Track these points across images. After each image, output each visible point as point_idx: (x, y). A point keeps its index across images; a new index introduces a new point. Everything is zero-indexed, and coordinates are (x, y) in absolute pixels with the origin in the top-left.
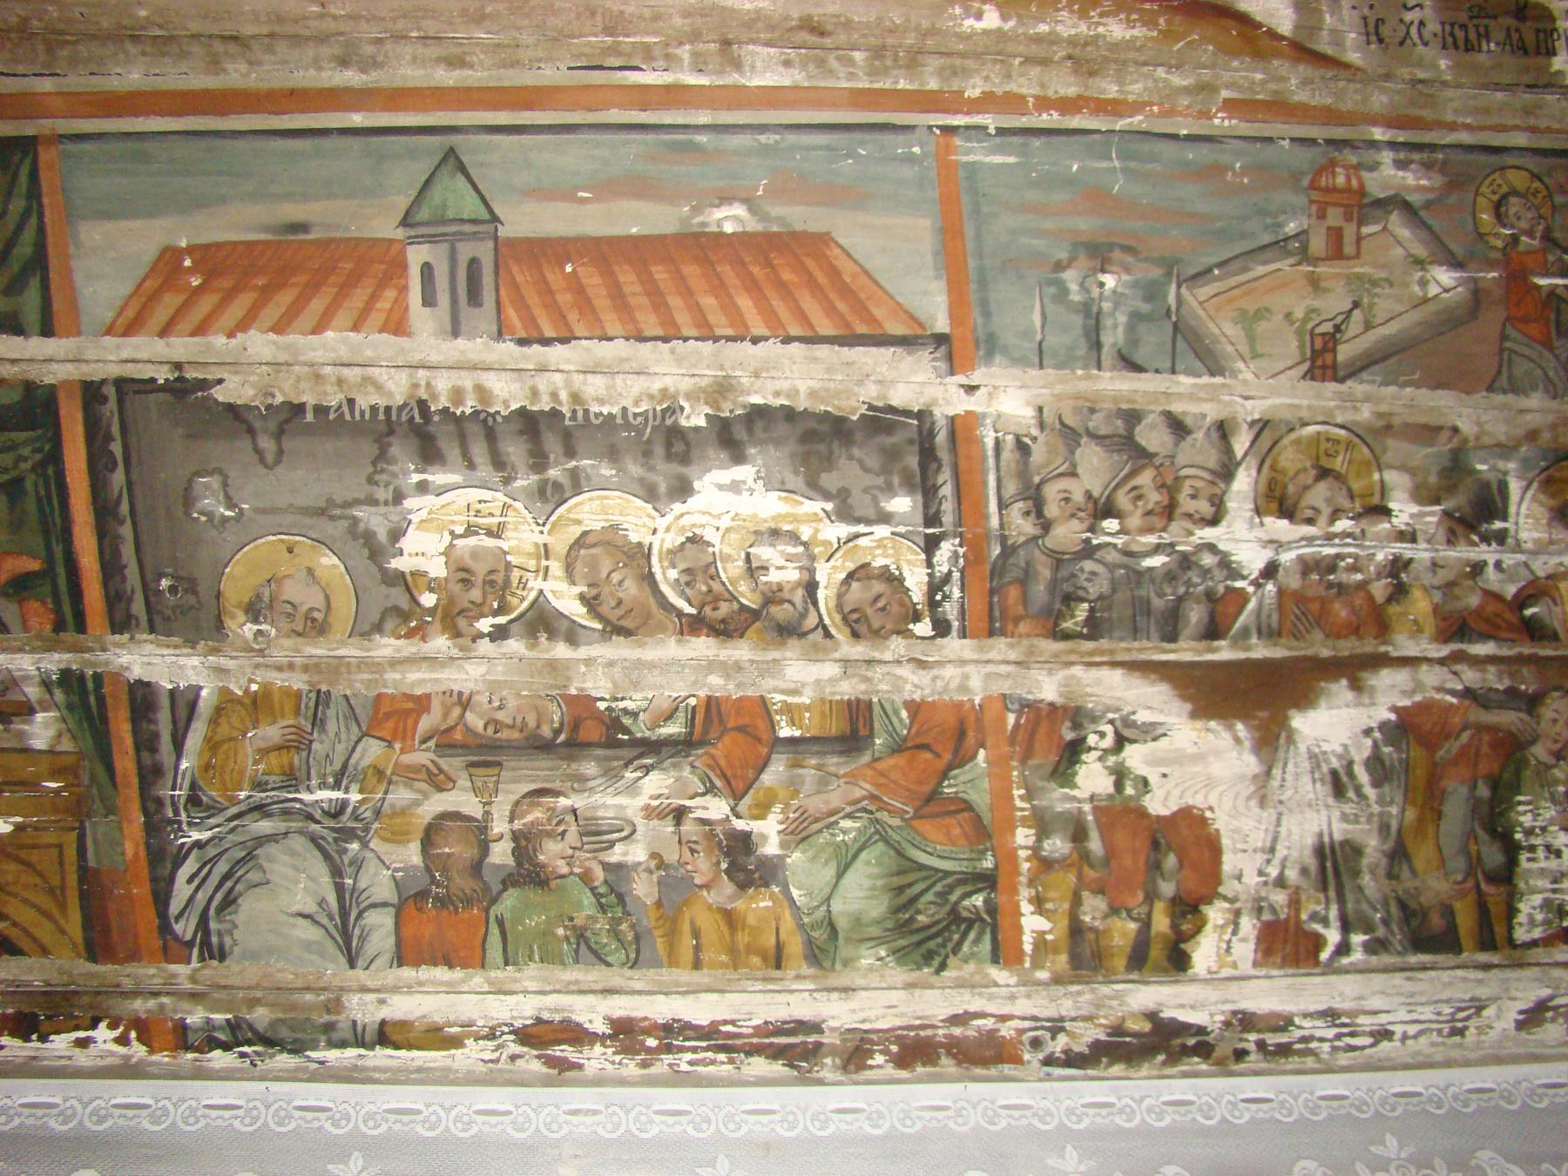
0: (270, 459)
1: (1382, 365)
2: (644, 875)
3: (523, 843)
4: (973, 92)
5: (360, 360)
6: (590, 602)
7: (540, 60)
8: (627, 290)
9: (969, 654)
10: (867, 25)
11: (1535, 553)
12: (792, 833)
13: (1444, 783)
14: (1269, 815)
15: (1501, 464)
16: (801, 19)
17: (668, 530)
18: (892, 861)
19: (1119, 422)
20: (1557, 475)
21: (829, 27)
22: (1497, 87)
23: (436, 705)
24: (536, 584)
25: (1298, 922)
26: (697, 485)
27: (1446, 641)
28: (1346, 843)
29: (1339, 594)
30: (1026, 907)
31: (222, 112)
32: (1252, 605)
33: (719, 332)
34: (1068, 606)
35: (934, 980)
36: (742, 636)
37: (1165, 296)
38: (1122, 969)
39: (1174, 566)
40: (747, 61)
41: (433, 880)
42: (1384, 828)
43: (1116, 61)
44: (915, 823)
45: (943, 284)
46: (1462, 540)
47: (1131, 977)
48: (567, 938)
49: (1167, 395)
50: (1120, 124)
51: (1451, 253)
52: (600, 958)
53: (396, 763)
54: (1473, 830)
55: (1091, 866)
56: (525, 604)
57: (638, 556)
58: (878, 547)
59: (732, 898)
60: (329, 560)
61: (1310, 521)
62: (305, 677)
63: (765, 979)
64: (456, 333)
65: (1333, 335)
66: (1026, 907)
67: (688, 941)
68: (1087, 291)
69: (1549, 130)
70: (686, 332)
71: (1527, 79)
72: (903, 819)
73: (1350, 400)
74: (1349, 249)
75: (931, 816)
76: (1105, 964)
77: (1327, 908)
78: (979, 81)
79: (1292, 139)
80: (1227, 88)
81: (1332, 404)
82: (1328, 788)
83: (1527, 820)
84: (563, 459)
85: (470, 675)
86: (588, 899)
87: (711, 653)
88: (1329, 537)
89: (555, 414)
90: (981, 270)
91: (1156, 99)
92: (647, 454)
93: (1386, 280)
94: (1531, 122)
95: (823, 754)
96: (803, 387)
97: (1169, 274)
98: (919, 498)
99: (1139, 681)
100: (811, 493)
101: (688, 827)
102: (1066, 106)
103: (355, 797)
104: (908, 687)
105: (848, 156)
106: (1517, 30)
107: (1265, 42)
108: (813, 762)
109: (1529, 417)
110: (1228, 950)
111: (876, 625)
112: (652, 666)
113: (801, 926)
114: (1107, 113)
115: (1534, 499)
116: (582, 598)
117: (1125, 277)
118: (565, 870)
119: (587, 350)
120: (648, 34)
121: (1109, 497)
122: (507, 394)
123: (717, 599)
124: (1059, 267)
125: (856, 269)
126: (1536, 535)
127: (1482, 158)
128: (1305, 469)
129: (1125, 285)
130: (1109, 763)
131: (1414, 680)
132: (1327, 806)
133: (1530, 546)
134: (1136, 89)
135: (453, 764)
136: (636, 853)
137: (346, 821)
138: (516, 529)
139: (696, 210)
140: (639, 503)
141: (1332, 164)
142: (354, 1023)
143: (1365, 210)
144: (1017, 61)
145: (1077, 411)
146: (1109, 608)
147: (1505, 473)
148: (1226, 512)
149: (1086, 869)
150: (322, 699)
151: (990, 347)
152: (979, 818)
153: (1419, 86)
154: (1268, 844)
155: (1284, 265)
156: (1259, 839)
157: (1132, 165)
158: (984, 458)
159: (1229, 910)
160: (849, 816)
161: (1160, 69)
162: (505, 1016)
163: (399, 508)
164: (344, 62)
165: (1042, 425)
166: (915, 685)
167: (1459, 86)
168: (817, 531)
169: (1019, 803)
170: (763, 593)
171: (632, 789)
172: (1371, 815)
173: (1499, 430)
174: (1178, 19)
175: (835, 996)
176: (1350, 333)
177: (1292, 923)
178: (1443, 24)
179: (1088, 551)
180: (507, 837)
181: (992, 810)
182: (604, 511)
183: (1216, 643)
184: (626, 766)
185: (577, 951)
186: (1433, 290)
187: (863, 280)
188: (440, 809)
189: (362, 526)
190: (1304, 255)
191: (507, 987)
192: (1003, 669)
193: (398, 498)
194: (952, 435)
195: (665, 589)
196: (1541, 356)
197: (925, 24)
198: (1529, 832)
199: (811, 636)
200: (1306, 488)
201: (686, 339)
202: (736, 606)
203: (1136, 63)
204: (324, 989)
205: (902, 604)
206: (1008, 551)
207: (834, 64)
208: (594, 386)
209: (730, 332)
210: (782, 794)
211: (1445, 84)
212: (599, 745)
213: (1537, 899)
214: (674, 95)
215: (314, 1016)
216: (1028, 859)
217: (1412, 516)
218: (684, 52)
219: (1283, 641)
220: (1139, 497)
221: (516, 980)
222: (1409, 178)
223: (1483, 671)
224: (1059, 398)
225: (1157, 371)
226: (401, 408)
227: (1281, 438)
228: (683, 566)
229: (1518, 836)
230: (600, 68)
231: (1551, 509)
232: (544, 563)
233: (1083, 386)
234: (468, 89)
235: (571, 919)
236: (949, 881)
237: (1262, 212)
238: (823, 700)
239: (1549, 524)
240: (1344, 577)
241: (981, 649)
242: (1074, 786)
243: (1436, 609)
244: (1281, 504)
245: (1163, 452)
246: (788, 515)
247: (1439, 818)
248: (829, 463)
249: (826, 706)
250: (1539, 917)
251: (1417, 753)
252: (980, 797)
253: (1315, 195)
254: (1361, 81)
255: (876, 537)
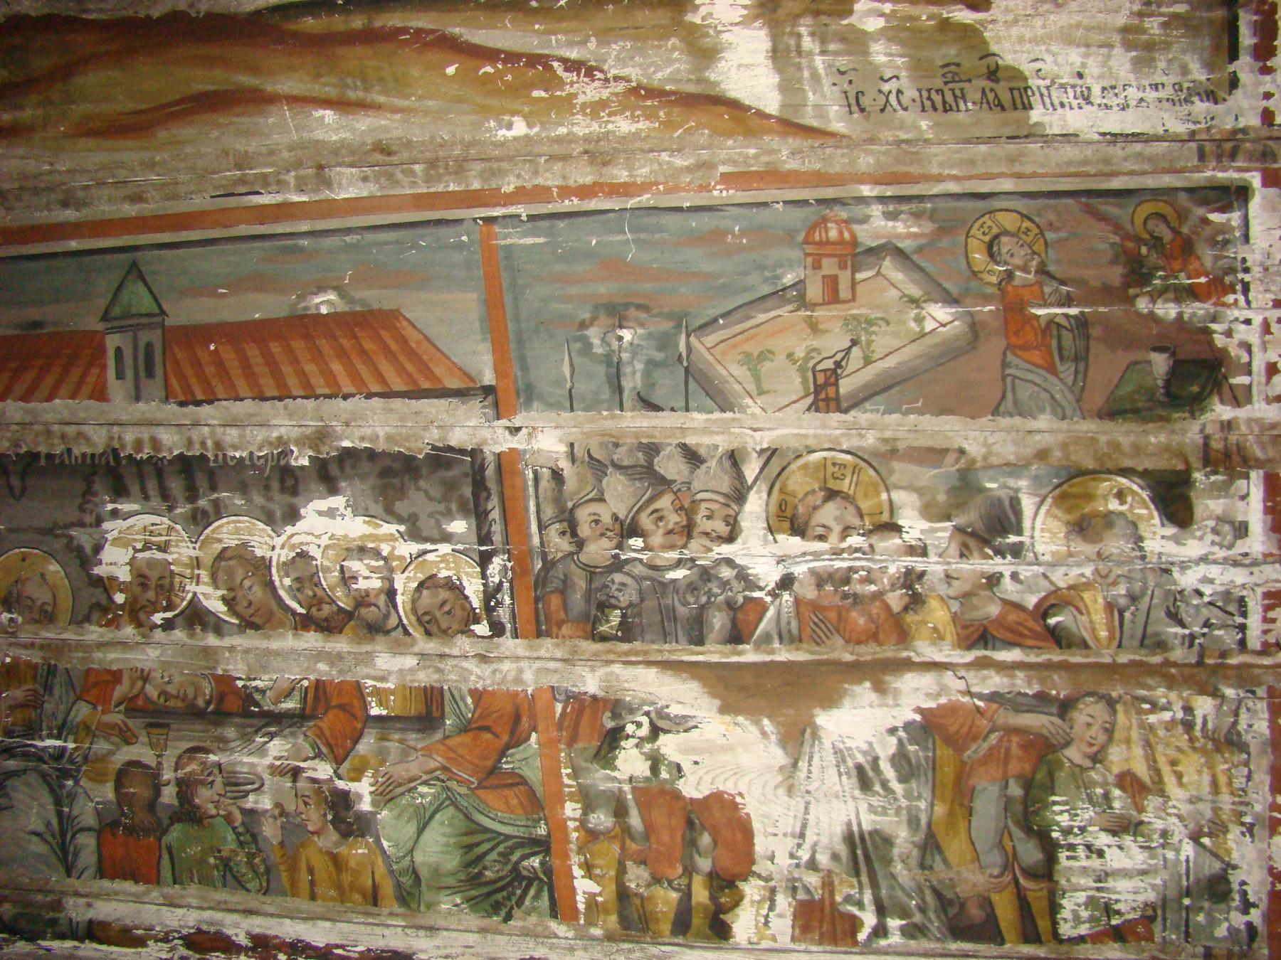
0: (17, 492)
1: (884, 395)
2: (271, 820)
3: (184, 788)
4: (508, 188)
5: (74, 420)
6: (229, 602)
7: (192, 193)
8: (253, 361)
9: (521, 652)
10: (423, 143)
11: (1053, 565)
12: (381, 794)
13: (973, 781)
14: (797, 804)
15: (1012, 482)
16: (373, 144)
17: (283, 547)
18: (462, 824)
19: (640, 455)
20: (1073, 490)
21: (394, 148)
22: (979, 140)
23: (126, 679)
24: (191, 587)
25: (833, 903)
26: (303, 511)
27: (970, 647)
28: (874, 833)
29: (855, 603)
30: (577, 872)
31: (24, 242)
32: (771, 613)
33: (319, 391)
34: (603, 612)
35: (503, 927)
36: (341, 632)
37: (677, 345)
38: (668, 933)
39: (694, 578)
40: (335, 179)
41: (123, 814)
42: (913, 822)
43: (625, 151)
44: (480, 792)
45: (488, 345)
46: (976, 554)
47: (676, 940)
48: (216, 867)
49: (683, 430)
50: (632, 203)
51: (947, 292)
52: (241, 884)
53: (99, 723)
54: (1006, 827)
55: (633, 839)
56: (185, 603)
57: (262, 567)
58: (441, 562)
59: (337, 844)
60: (54, 567)
61: (822, 538)
62: (42, 654)
63: (367, 914)
64: (138, 399)
65: (834, 371)
66: (577, 872)
67: (305, 877)
68: (609, 345)
69: (1034, 175)
70: (295, 393)
71: (1009, 131)
72: (469, 788)
73: (858, 429)
74: (844, 293)
75: (497, 787)
76: (652, 927)
77: (861, 892)
78: (512, 179)
79: (785, 202)
80: (724, 163)
81: (838, 432)
82: (855, 780)
83: (1064, 820)
84: (208, 492)
85: (149, 657)
86: (231, 837)
87: (319, 645)
88: (837, 553)
89: (203, 457)
90: (519, 333)
91: (662, 179)
92: (267, 488)
93: (882, 319)
94: (1017, 168)
95: (403, 730)
96: (381, 433)
97: (679, 326)
98: (473, 521)
99: (672, 679)
100: (388, 518)
101: (301, 784)
102: (585, 192)
103: (71, 745)
104: (473, 678)
105: (412, 247)
106: (992, 90)
107: (756, 121)
108: (397, 736)
109: (1038, 437)
110: (766, 923)
111: (444, 625)
112: (277, 653)
113: (392, 872)
114: (619, 194)
115: (1048, 512)
116: (223, 599)
117: (640, 331)
118: (214, 812)
119: (226, 408)
120: (266, 166)
121: (633, 518)
122: (172, 442)
123: (320, 602)
124: (583, 325)
125: (421, 337)
126: (1054, 548)
127: (971, 204)
128: (814, 491)
129: (641, 338)
130: (645, 750)
131: (939, 683)
132: (854, 798)
133: (1048, 558)
134: (643, 173)
135: (135, 724)
136: (265, 803)
137: (65, 764)
138: (177, 546)
139: (302, 297)
140: (261, 525)
141: (825, 220)
142: (71, 920)
143: (859, 258)
144: (543, 160)
145: (602, 445)
146: (640, 614)
147: (1017, 490)
148: (741, 531)
149: (628, 842)
150: (52, 670)
151: (529, 395)
152: (533, 792)
153: (904, 146)
154: (798, 830)
155: (783, 311)
156: (790, 824)
157: (643, 236)
158: (525, 488)
159: (764, 887)
160: (425, 783)
161: (663, 154)
162: (174, 924)
163: (98, 530)
164: (65, 204)
165: (572, 457)
166: (479, 676)
167: (942, 143)
168: (394, 548)
169: (566, 781)
170: (355, 598)
171: (262, 751)
172: (899, 809)
173: (1007, 450)
174: (676, 110)
175: (422, 933)
176: (849, 369)
177: (827, 903)
178: (920, 91)
179: (617, 565)
180: (173, 783)
181: (544, 785)
182: (237, 531)
183: (740, 647)
184: (256, 732)
185: (224, 877)
186: (929, 325)
187: (426, 344)
188: (127, 758)
189: (75, 542)
190: (802, 301)
191: (177, 901)
192: (552, 665)
193: (99, 521)
194: (499, 468)
195: (282, 593)
196: (1045, 380)
197: (467, 137)
198: (1067, 831)
199: (393, 634)
200: (815, 508)
201: (295, 398)
202: (335, 608)
203: (643, 151)
204: (50, 891)
205: (464, 609)
206: (549, 565)
207: (400, 176)
208: (232, 434)
209: (327, 391)
210: (373, 761)
211: (926, 141)
212: (237, 715)
213: (1081, 897)
214: (284, 211)
215: (43, 913)
216: (576, 829)
217: (922, 532)
218: (291, 178)
219: (804, 645)
220: (661, 519)
221: (182, 897)
222: (900, 227)
223: (1012, 677)
224: (588, 435)
225: (672, 409)
226: (102, 455)
227: (789, 464)
228: (295, 575)
229: (1055, 835)
230: (232, 195)
231: (1068, 523)
232: (197, 572)
233: (609, 425)
234: (144, 218)
235: (219, 851)
236: (510, 843)
237: (762, 268)
238: (404, 686)
239: (1066, 537)
240: (859, 588)
241: (531, 648)
242: (615, 768)
243: (955, 617)
244: (792, 524)
245: (680, 479)
246: (371, 535)
247: (971, 815)
248: (401, 493)
249: (407, 691)
250: (1085, 914)
251: (945, 752)
252: (533, 773)
253: (809, 248)
254: (848, 147)
255: (440, 553)
